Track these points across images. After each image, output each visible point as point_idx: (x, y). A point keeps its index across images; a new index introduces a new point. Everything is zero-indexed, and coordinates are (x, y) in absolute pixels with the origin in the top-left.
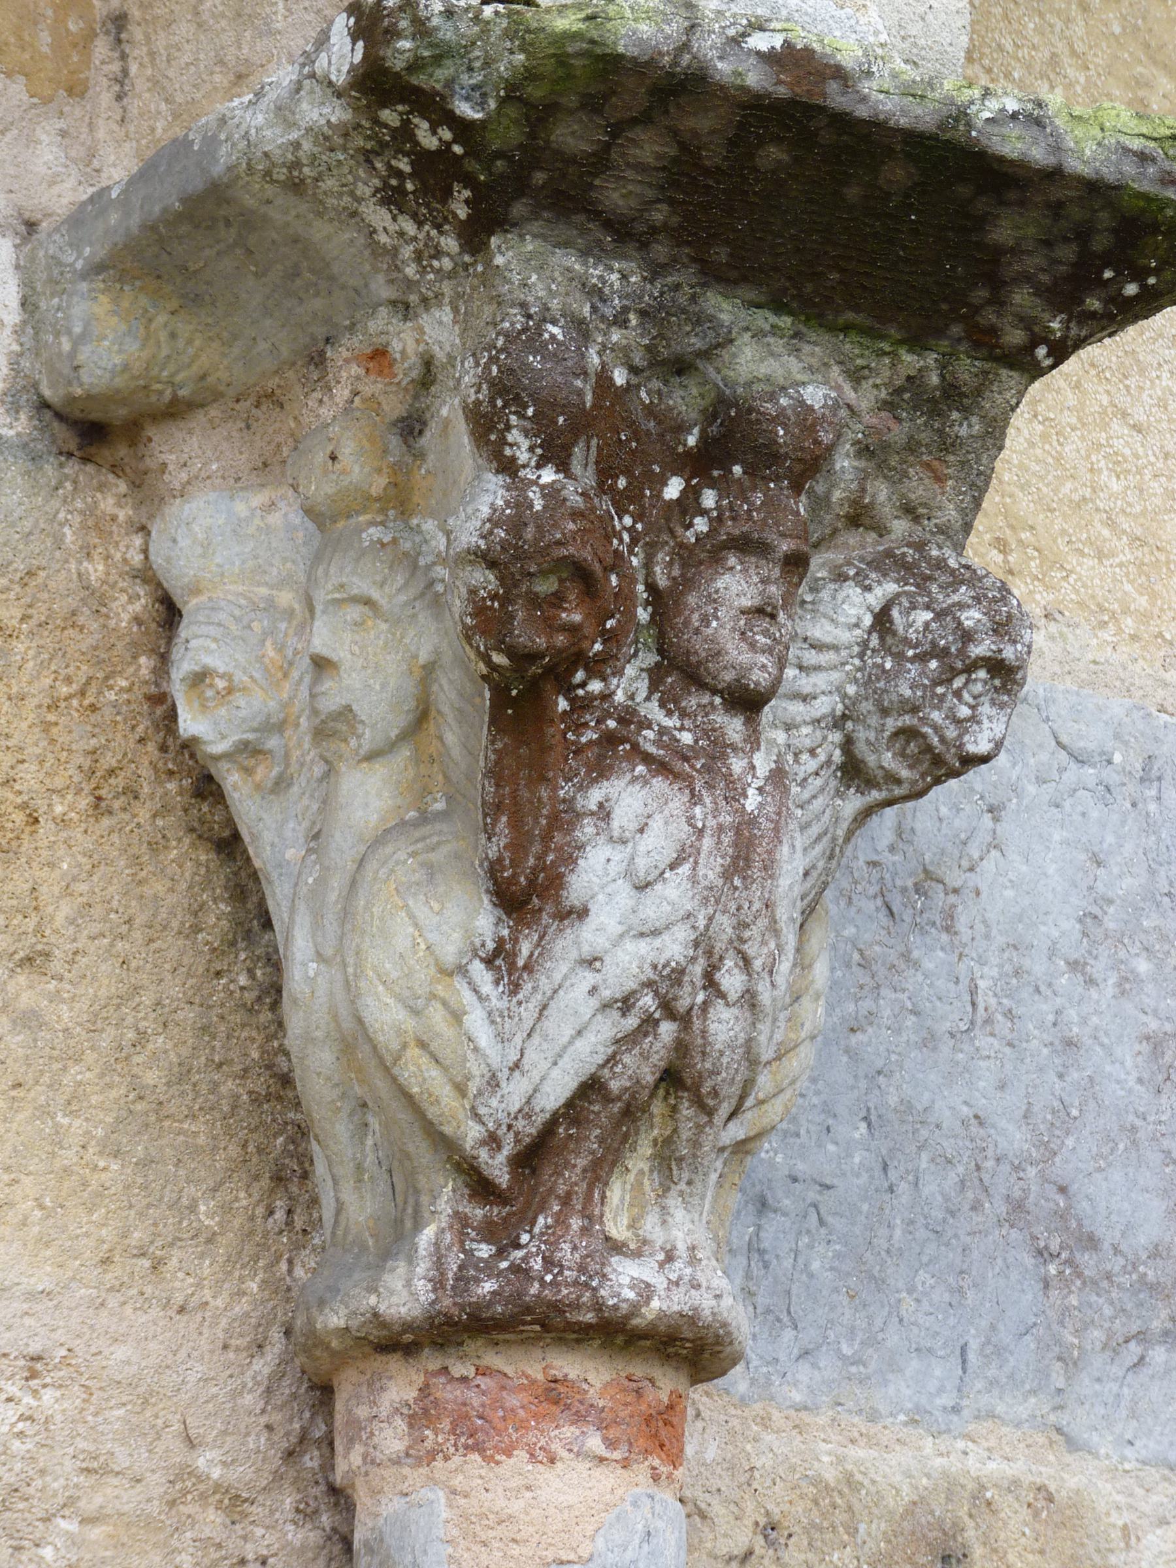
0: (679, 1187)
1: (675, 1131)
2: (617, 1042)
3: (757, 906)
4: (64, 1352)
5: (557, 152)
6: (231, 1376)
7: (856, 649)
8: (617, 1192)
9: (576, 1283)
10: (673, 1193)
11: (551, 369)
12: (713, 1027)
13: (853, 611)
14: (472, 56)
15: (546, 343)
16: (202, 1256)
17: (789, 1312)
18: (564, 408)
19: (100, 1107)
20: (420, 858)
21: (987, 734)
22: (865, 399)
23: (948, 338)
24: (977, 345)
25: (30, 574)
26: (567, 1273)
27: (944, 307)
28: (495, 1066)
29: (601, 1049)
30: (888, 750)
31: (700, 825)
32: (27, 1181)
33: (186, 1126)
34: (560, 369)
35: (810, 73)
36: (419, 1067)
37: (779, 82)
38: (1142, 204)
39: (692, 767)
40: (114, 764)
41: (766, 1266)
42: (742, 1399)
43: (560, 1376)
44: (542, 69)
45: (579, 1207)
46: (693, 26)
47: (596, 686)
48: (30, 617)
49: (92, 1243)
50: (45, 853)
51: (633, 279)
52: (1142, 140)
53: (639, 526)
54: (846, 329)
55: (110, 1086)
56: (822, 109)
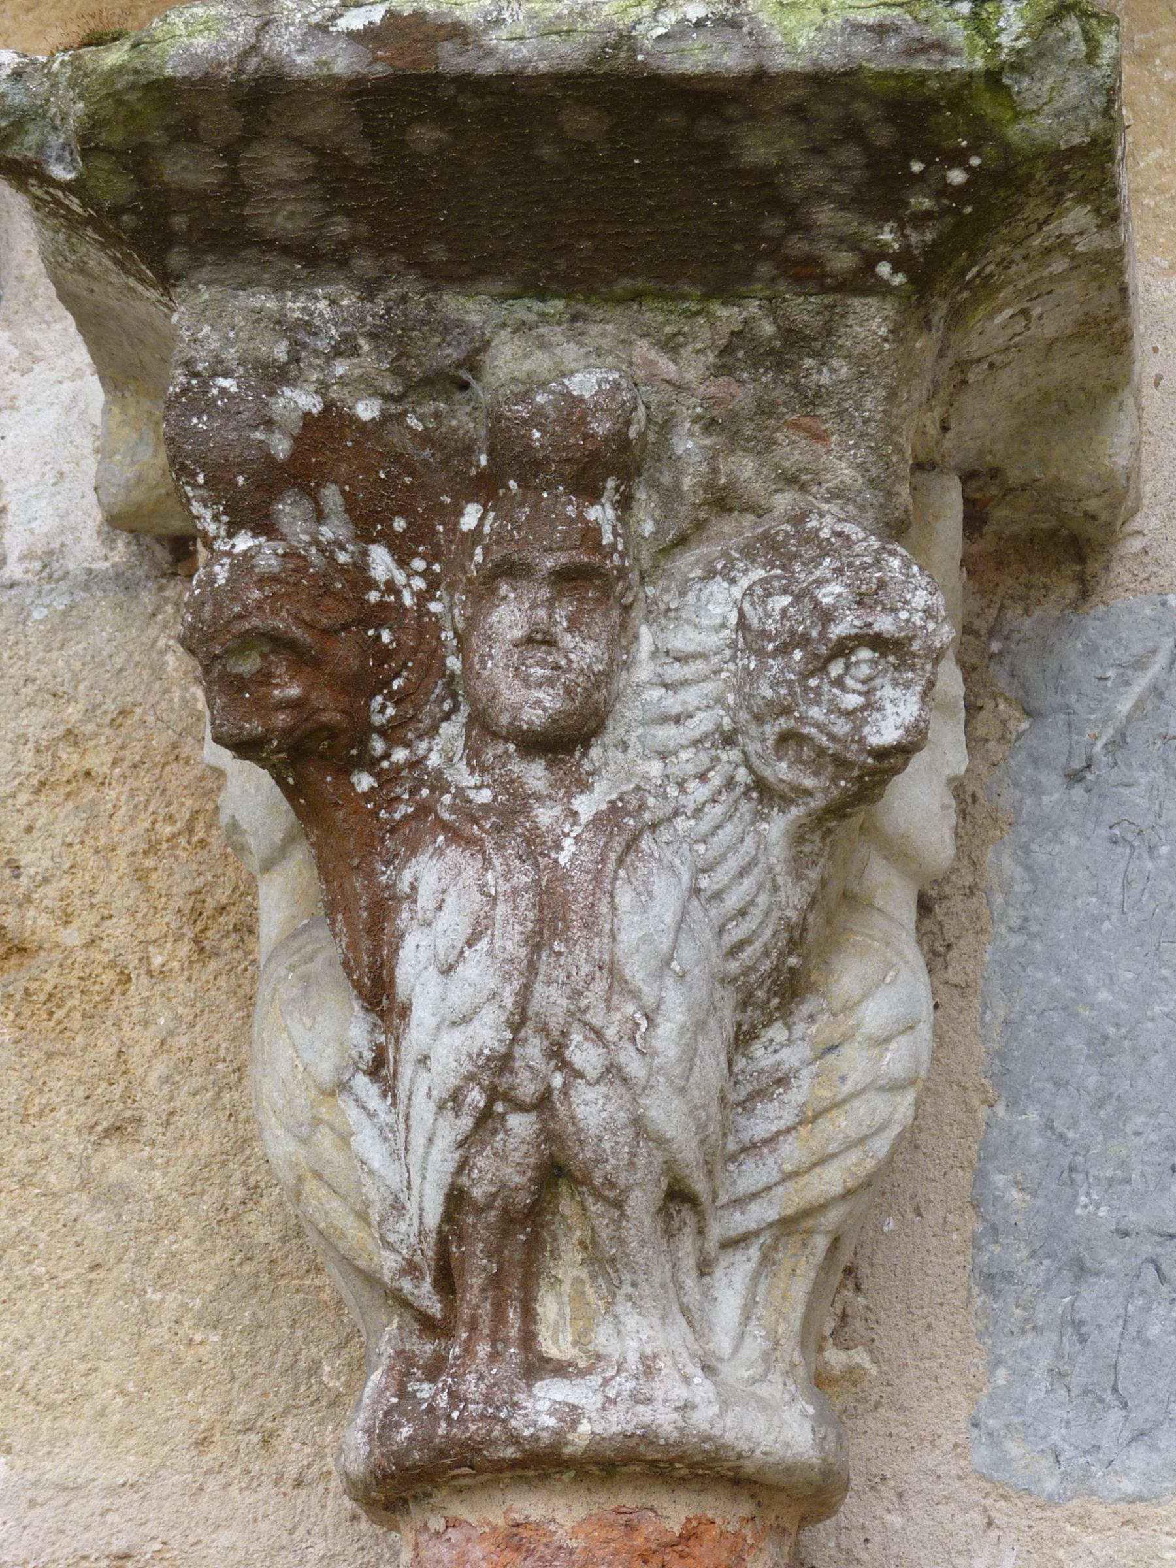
0: (623, 1291)
1: (593, 1230)
2: (460, 1145)
3: (585, 969)
4: (157, 1546)
5: (181, 191)
6: (362, 1549)
7: (728, 653)
8: (549, 1307)
9: (482, 1417)
10: (620, 1299)
11: (219, 428)
12: (580, 1111)
13: (719, 611)
14: (50, 114)
15: (215, 399)
16: (322, 1422)
17: (1115, 1390)
18: (240, 468)
19: (200, 1275)
20: (299, 971)
21: (892, 720)
22: (691, 367)
23: (759, 280)
24: (798, 280)
25: (123, 713)
26: (472, 1407)
27: (738, 247)
28: (394, 1187)
29: (449, 1156)
30: (780, 759)
31: (493, 892)
32: (107, 1367)
33: (308, 1282)
34: (232, 425)
35: (417, 41)
36: (319, 1199)
37: (376, 60)
38: (892, 83)
39: (481, 828)
40: (224, 900)
41: (1083, 1339)
42: (1050, 1497)
43: (521, 1519)
44: (103, 113)
45: (487, 1331)
46: (267, 24)
47: (400, 755)
48: (122, 760)
49: (184, 1424)
50: (136, 1011)
51: (345, 302)
52: (882, 10)
53: (437, 568)
54: (637, 297)
55: (212, 1251)
56: (438, 76)
